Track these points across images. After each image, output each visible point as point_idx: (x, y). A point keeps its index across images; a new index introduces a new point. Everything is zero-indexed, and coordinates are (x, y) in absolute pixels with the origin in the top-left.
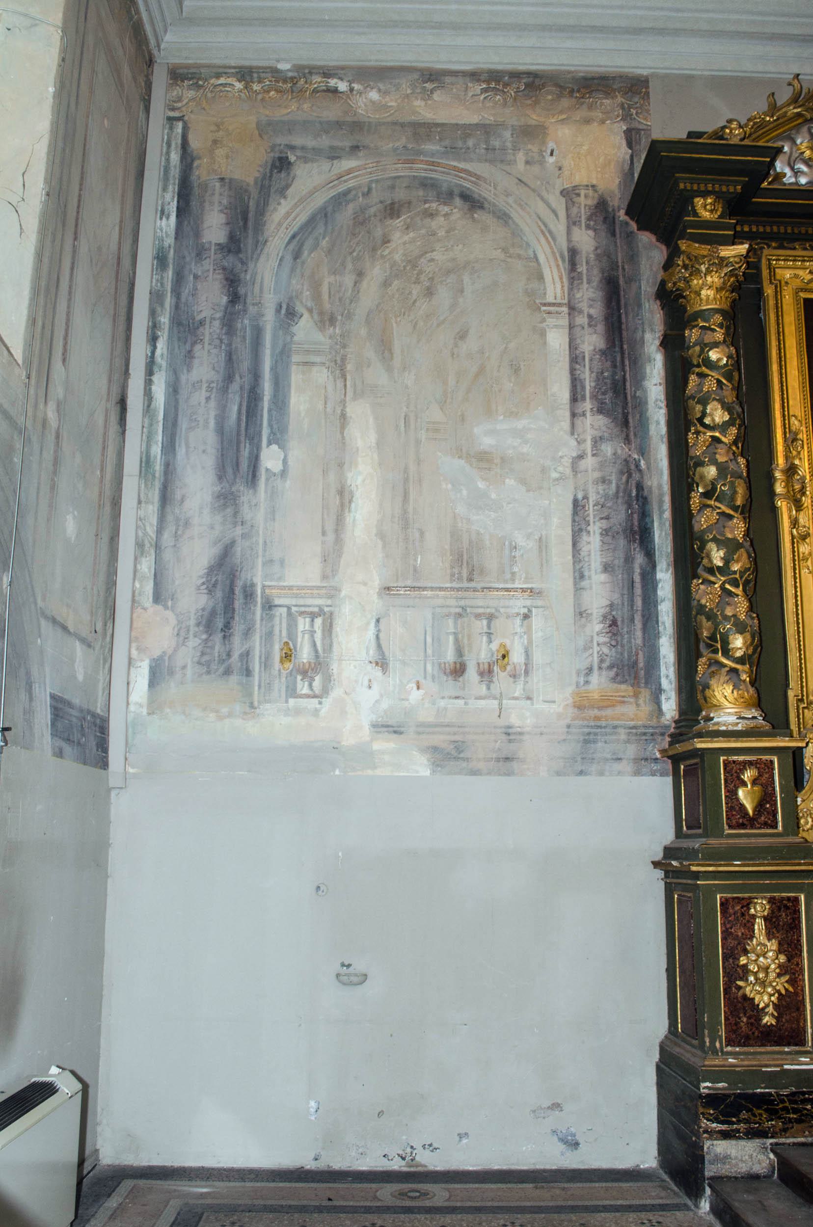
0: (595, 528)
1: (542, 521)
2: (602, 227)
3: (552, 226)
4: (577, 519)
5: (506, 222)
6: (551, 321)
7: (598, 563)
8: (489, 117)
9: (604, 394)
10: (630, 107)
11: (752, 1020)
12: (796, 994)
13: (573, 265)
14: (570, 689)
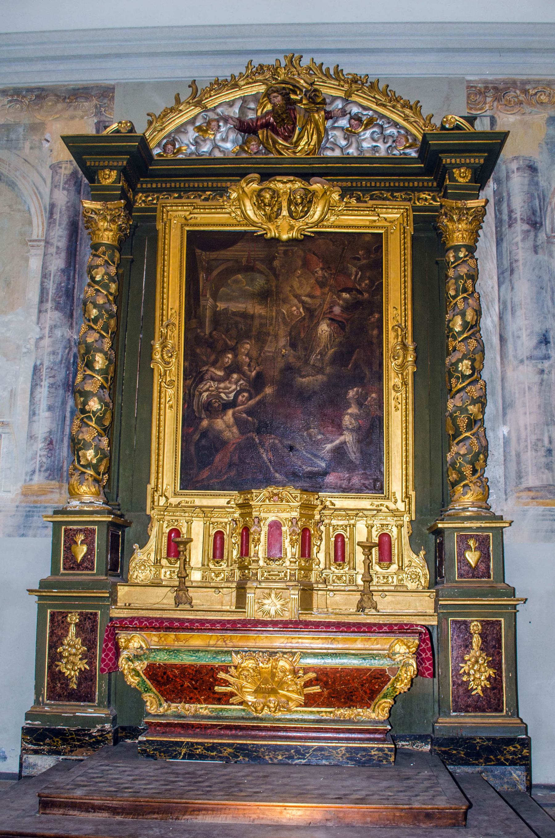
0: (46, 383)
1: (14, 380)
2: (73, 188)
3: (41, 189)
4: (35, 378)
5: (13, 188)
6: (33, 251)
7: (45, 405)
8: (10, 119)
9: (60, 297)
10: (101, 106)
11: (64, 686)
12: (91, 670)
13: (51, 213)
14: (20, 484)
